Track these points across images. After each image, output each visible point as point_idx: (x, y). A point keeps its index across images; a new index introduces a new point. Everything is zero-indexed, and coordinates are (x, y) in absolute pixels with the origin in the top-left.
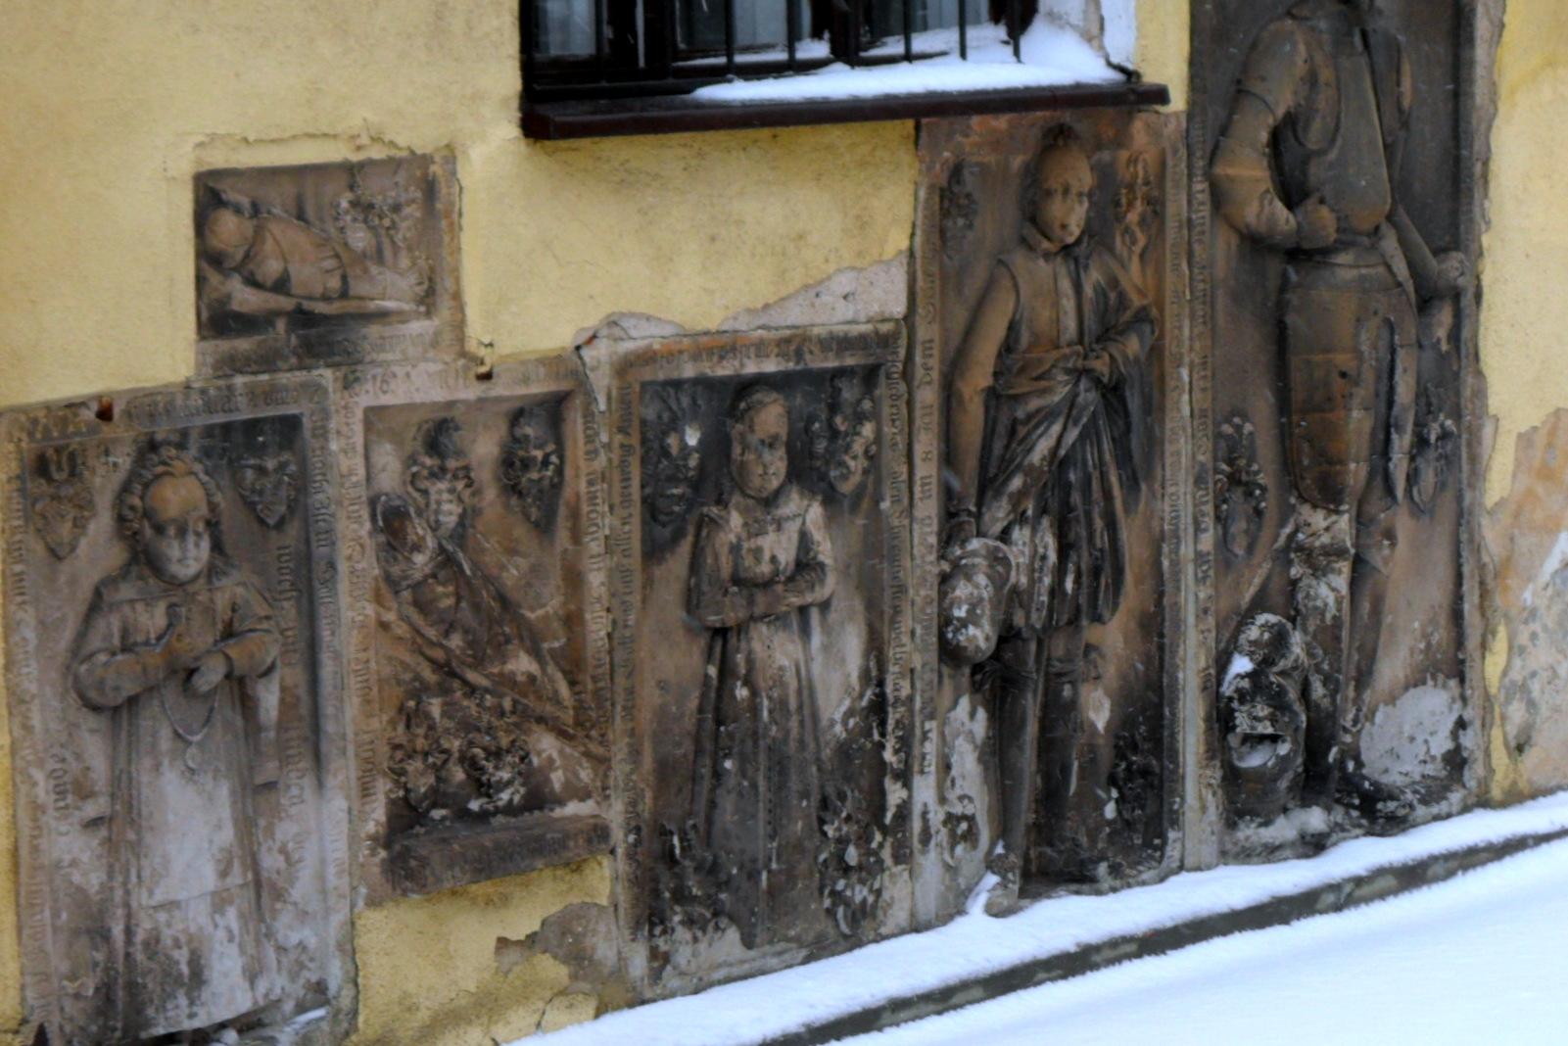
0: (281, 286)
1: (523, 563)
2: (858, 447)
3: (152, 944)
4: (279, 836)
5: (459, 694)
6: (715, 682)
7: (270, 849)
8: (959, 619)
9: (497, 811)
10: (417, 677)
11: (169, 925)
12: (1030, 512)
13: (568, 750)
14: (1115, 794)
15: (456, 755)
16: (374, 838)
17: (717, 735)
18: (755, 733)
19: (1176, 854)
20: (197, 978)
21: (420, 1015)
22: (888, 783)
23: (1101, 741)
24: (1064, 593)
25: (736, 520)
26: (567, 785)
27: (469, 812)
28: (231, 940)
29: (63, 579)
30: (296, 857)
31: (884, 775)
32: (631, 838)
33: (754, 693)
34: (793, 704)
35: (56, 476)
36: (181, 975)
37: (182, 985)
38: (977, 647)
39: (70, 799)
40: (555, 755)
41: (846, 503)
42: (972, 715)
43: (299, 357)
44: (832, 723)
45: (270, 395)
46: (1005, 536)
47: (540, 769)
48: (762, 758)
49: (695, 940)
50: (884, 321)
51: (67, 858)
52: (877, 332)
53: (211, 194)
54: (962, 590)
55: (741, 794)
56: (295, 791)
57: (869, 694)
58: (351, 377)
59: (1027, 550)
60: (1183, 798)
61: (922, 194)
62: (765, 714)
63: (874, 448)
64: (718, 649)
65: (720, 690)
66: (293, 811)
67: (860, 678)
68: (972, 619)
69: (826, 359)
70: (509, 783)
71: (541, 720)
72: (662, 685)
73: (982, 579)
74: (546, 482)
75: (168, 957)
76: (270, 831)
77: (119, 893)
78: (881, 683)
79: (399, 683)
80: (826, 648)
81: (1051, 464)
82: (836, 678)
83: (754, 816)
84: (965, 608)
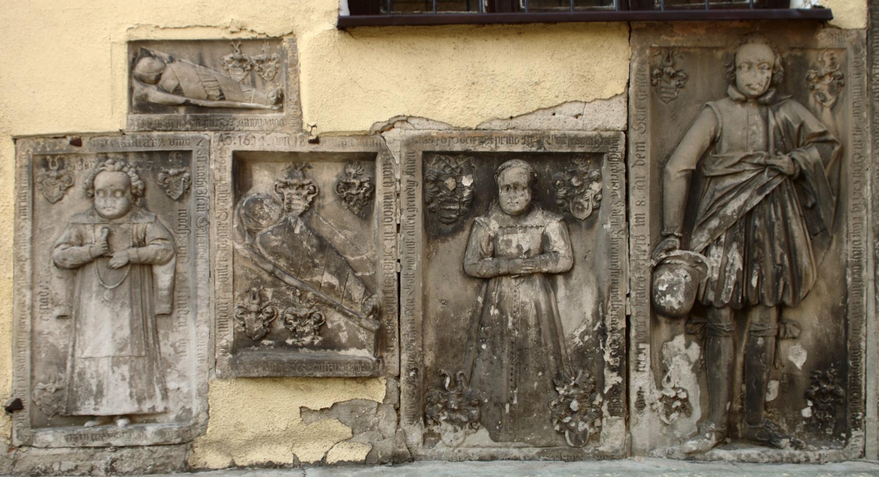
0: (178, 91)
1: (349, 234)
2: (589, 194)
3: (81, 375)
4: (171, 339)
5: (284, 288)
6: (481, 305)
7: (165, 344)
8: (661, 291)
9: (303, 346)
10: (259, 277)
11: (89, 368)
12: (723, 240)
13: (351, 323)
14: (810, 403)
15: (280, 316)
16: (226, 348)
17: (478, 330)
18: (502, 333)
19: (860, 444)
20: (99, 394)
21: (246, 434)
22: (606, 372)
23: (799, 373)
24: (752, 287)
25: (494, 225)
26: (349, 339)
27: (286, 344)
28: (124, 379)
29: (54, 212)
30: (181, 349)
31: (603, 368)
32: (412, 374)
33: (502, 312)
34: (532, 321)
35: (51, 168)
36: (91, 391)
37: (92, 395)
38: (672, 308)
39: (50, 306)
40: (343, 324)
41: (584, 224)
42: (687, 346)
43: (192, 125)
44: (573, 337)
45: (173, 141)
46: (706, 251)
47: (332, 330)
48: (507, 347)
49: (456, 431)
50: (607, 130)
51: (46, 331)
52: (601, 136)
53: (139, 49)
54: (666, 276)
55: (492, 363)
56: (182, 320)
57: (598, 324)
58: (225, 136)
59: (720, 260)
60: (865, 414)
61: (635, 65)
62: (510, 324)
63: (599, 196)
64: (484, 289)
65: (483, 309)
66: (181, 329)
67: (593, 315)
68: (670, 290)
69: (561, 147)
70: (308, 334)
71: (331, 306)
72: (445, 303)
73: (683, 272)
74: (361, 196)
75: (88, 382)
76: (166, 336)
77: (70, 350)
78: (604, 319)
79: (247, 279)
80: (569, 298)
81: (738, 215)
82: (575, 314)
83: (500, 375)
84: (666, 286)
